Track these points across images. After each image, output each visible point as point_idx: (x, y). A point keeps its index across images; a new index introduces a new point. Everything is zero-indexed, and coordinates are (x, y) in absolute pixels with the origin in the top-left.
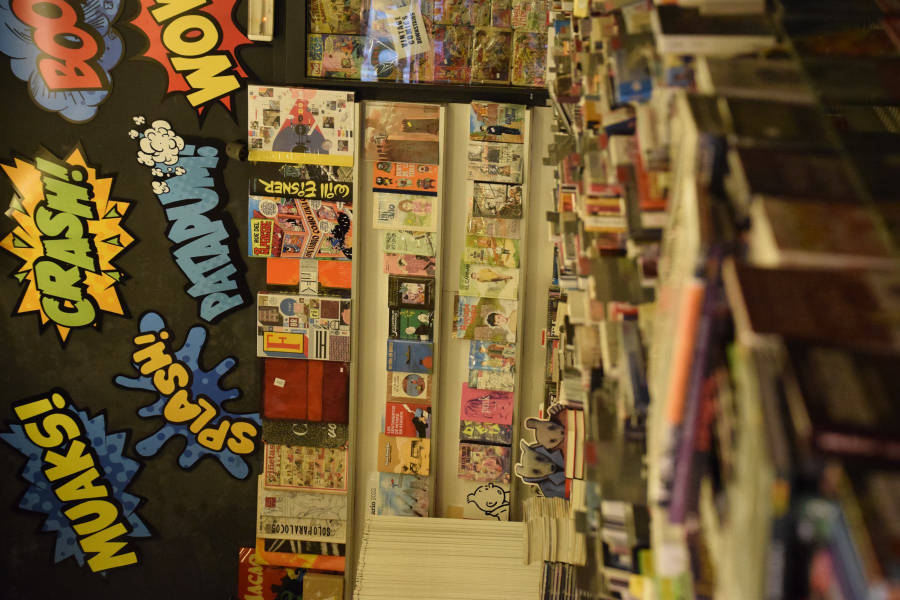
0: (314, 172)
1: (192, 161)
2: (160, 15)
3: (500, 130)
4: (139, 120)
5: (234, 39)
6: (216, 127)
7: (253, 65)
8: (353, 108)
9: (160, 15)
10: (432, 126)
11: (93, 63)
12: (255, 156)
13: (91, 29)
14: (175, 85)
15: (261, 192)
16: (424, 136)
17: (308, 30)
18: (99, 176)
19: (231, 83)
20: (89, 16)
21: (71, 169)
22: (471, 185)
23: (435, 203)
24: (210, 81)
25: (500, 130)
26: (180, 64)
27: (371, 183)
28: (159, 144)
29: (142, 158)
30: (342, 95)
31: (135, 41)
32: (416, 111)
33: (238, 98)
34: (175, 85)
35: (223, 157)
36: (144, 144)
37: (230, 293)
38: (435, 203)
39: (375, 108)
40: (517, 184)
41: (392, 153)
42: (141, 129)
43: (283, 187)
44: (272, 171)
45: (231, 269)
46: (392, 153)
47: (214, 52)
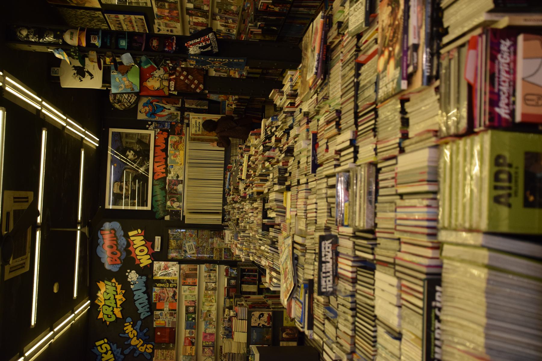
0: (168, 281)
1: (140, 280)
2: (135, 247)
3: (211, 270)
4: (128, 271)
5: (151, 251)
6: (146, 272)
7: (156, 257)
8: (178, 266)
9: (135, 247)
10: (196, 270)
11: (119, 258)
12: (154, 278)
13: (119, 251)
14: (137, 262)
15: (156, 286)
16: (194, 272)
17: (168, 248)
18: (119, 284)
19: (150, 261)
20: (119, 248)
21: (112, 283)
22: (205, 283)
23: (197, 287)
24: (145, 261)
25: (211, 270)
26: (138, 257)
27: (181, 283)
28: (133, 276)
29: (129, 280)
30: (176, 263)
31: (129, 252)
32: (192, 266)
33: (152, 265)
34: (137, 262)
35: (147, 279)
36: (129, 276)
37: (148, 312)
38: (197, 287)
39: (183, 266)
40: (215, 282)
41: (187, 276)
42: (129, 273)
43: (161, 285)
44: (159, 281)
45: (164, 166)
46: (187, 276)
47: (146, 254)
